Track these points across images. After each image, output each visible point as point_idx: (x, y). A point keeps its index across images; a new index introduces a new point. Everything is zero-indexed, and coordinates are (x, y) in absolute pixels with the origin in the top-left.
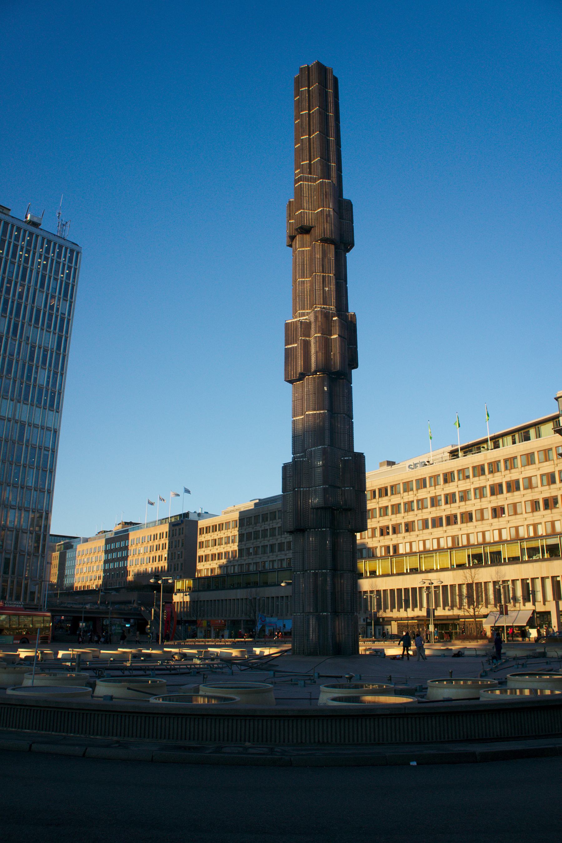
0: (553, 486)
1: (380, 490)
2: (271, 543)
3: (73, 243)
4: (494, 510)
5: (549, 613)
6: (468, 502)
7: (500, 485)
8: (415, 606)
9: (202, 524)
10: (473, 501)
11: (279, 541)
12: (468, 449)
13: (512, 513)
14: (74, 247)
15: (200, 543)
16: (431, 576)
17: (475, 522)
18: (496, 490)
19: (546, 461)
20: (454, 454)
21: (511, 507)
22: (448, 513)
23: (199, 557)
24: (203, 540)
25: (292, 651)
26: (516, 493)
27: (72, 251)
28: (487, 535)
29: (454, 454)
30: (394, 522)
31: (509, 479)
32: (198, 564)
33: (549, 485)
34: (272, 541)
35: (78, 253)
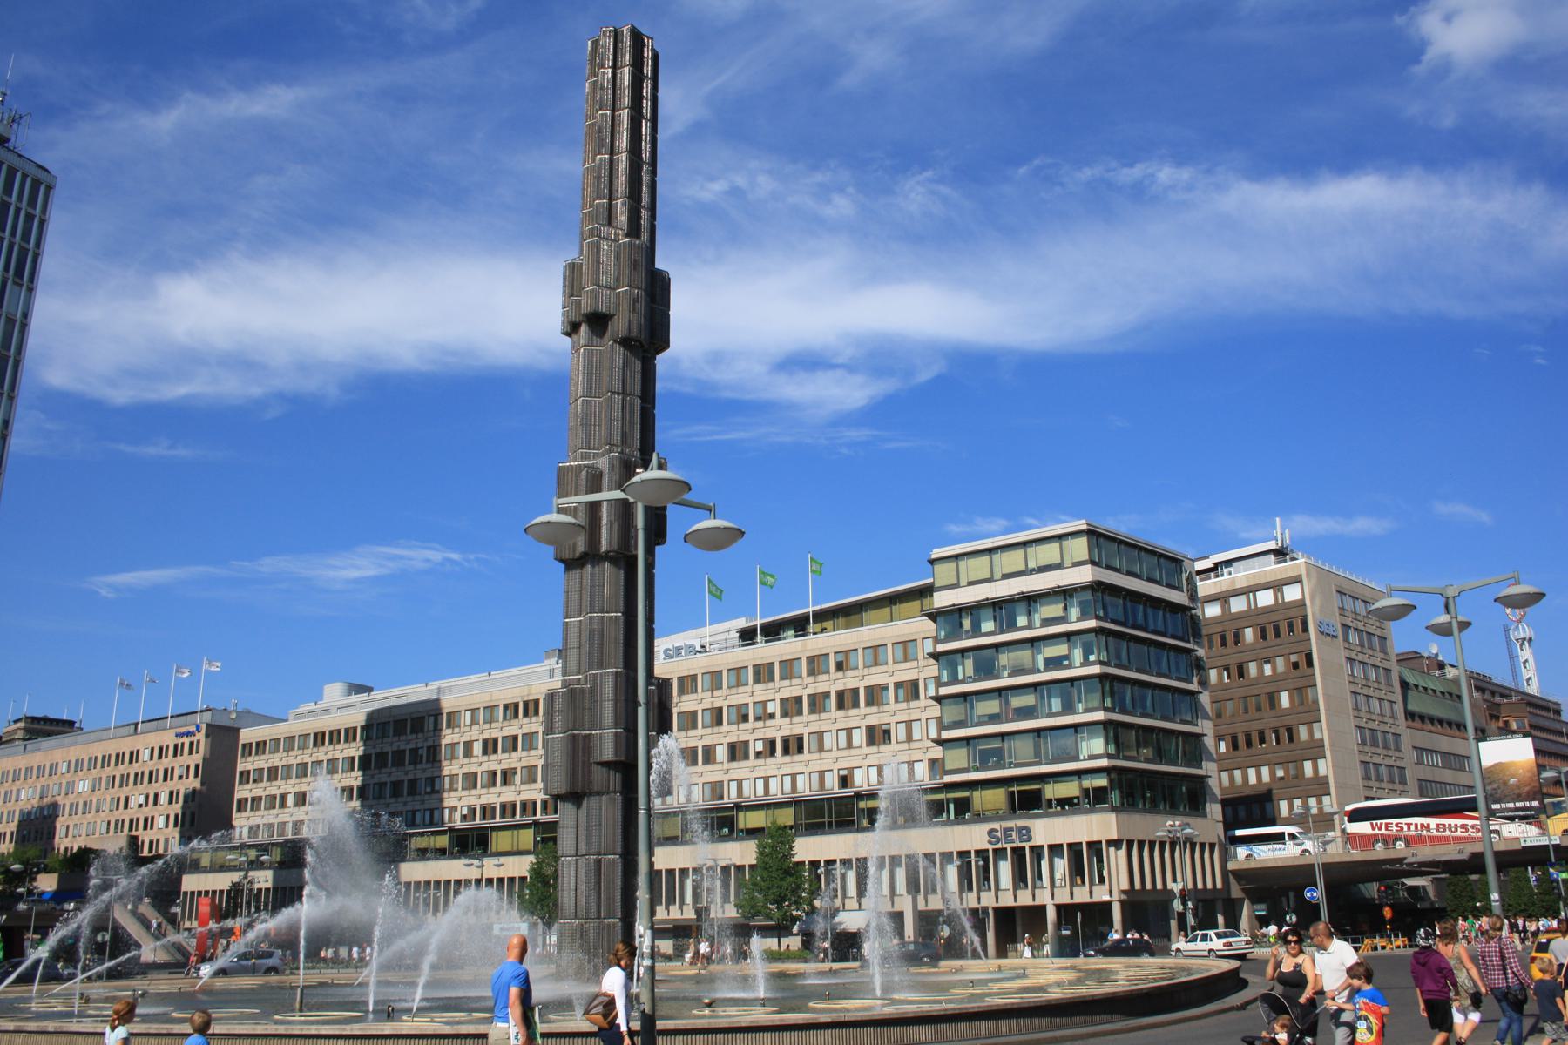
0: (914, 704)
1: (526, 704)
2: (393, 779)
3: (39, 166)
4: (733, 748)
5: (1043, 908)
6: (823, 716)
7: (799, 700)
8: (671, 900)
9: (248, 735)
10: (893, 706)
11: (411, 776)
12: (773, 631)
13: (814, 747)
14: (41, 175)
15: (242, 773)
16: (473, 874)
17: (806, 756)
18: (791, 707)
19: (906, 660)
20: (747, 636)
21: (814, 738)
22: (786, 732)
23: (239, 801)
24: (249, 767)
25: (1531, 894)
26: (853, 712)
27: (36, 183)
28: (773, 784)
29: (747, 636)
30: (505, 766)
31: (841, 687)
32: (235, 815)
33: (907, 700)
34: (397, 775)
35: (49, 188)
